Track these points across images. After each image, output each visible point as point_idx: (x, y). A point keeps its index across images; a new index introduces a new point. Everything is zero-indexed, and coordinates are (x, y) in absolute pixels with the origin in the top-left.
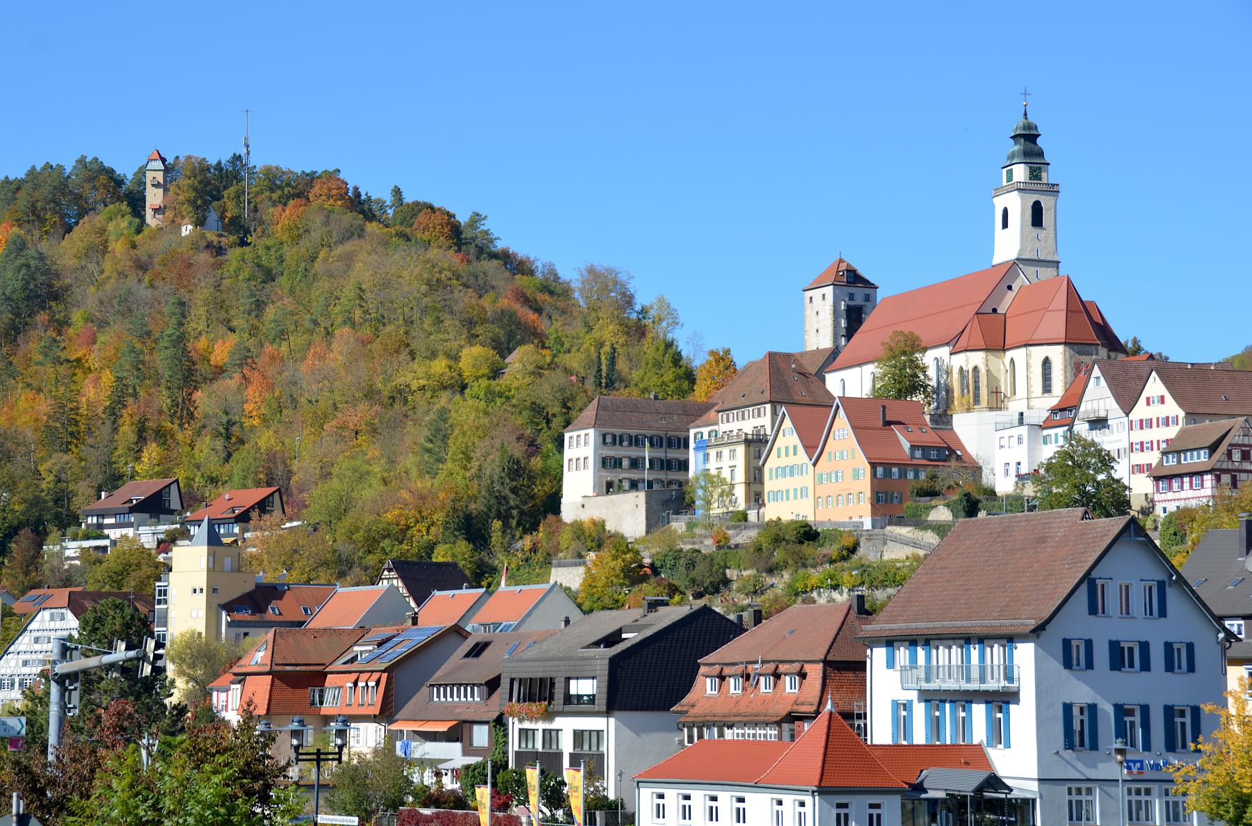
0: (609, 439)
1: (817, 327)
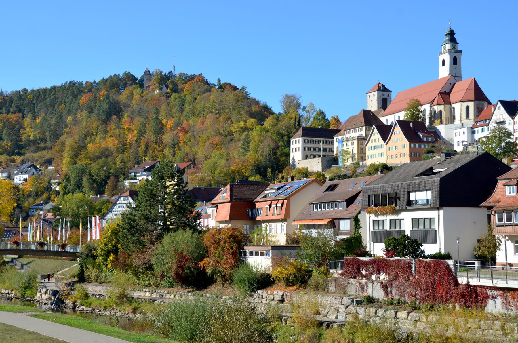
0: (306, 141)
1: (371, 105)
